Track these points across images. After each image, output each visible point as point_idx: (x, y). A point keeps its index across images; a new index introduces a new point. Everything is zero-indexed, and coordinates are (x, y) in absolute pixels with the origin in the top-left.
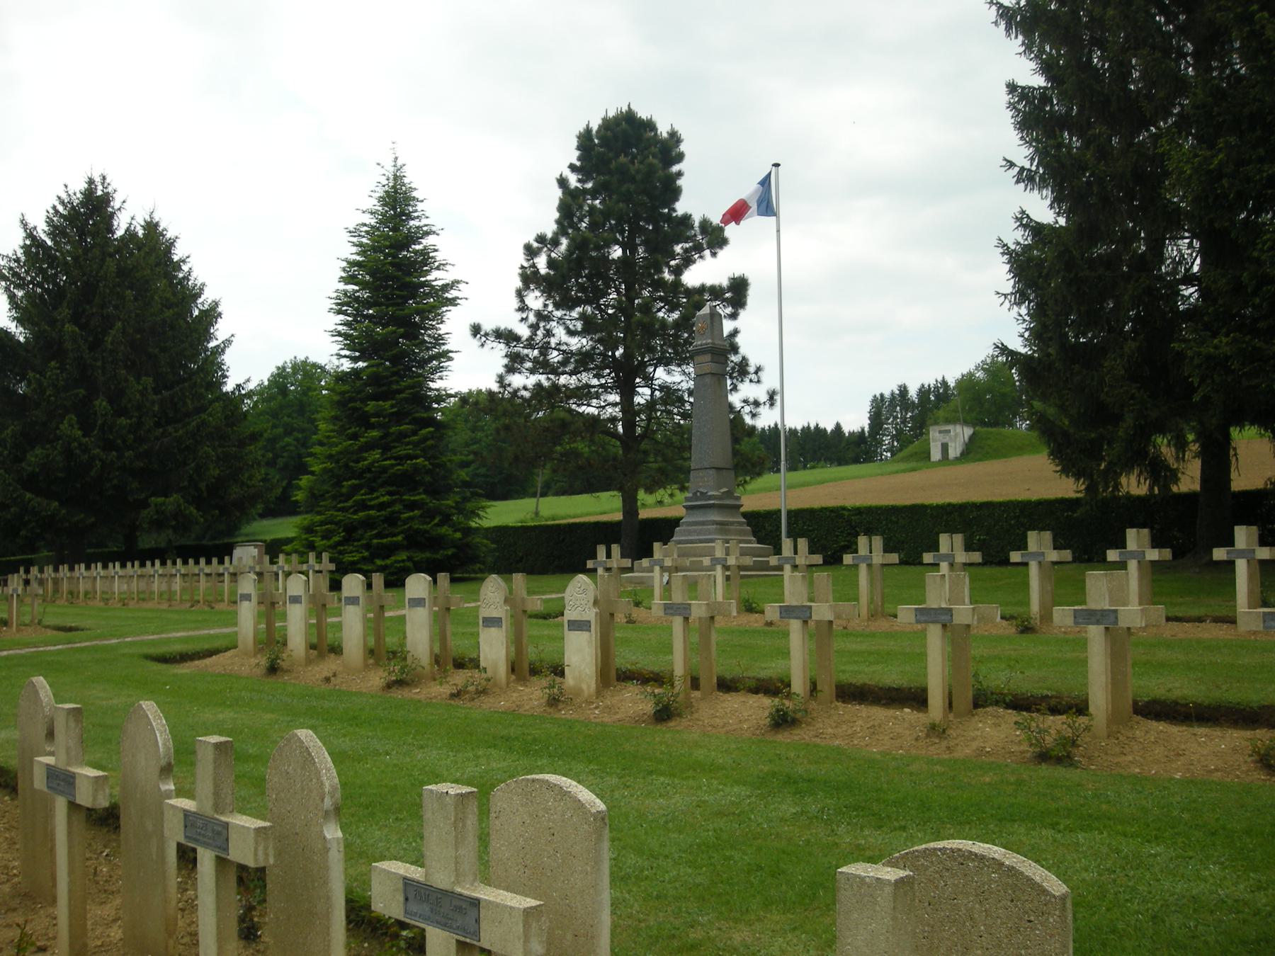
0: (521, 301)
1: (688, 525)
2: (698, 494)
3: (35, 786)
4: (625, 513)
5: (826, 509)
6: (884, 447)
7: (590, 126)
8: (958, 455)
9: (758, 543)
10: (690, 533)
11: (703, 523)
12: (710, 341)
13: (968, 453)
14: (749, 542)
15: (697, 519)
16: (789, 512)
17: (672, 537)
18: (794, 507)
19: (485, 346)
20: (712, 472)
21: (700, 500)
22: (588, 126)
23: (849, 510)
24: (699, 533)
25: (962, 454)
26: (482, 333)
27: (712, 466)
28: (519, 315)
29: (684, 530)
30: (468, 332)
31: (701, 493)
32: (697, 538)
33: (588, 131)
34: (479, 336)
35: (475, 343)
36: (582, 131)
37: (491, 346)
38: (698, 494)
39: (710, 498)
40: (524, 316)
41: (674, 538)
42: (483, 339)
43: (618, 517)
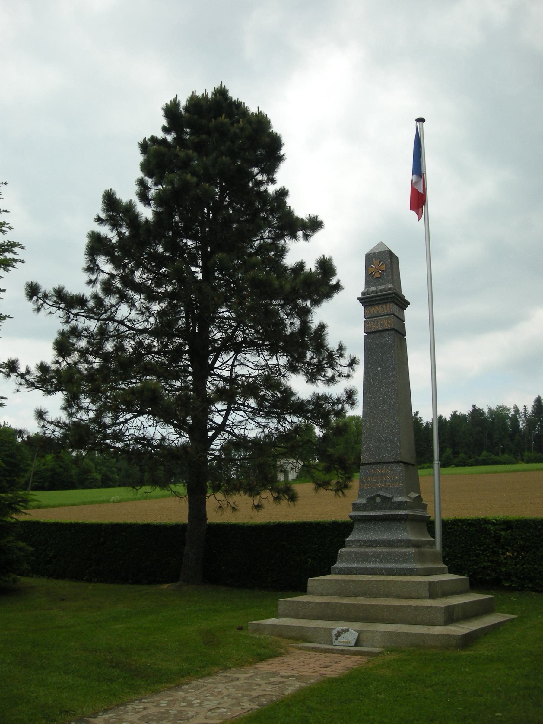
0: (91, 261)
1: (361, 546)
2: (378, 500)
3: (188, 377)
4: (191, 516)
5: (460, 521)
6: (232, 472)
7: (178, 99)
8: (295, 478)
9: (450, 572)
10: (366, 558)
11: (389, 544)
12: (390, 286)
13: (301, 477)
14: (440, 572)
15: (385, 537)
16: (445, 524)
17: (335, 562)
18: (449, 516)
19: (42, 309)
20: (399, 468)
21: (381, 509)
22: (175, 100)
23: (493, 524)
24: (384, 559)
25: (297, 477)
26: (40, 295)
27: (399, 458)
28: (86, 277)
29: (355, 553)
30: (22, 293)
31: (384, 499)
32: (382, 566)
33: (175, 104)
34: (35, 298)
35: (30, 305)
36: (169, 103)
37: (48, 311)
38: (378, 500)
39: (400, 505)
40: (93, 277)
41: (337, 565)
42: (40, 302)
43: (184, 520)
